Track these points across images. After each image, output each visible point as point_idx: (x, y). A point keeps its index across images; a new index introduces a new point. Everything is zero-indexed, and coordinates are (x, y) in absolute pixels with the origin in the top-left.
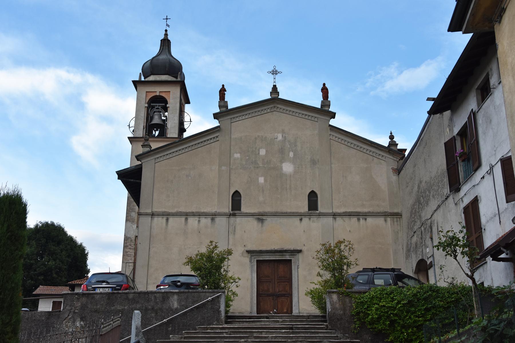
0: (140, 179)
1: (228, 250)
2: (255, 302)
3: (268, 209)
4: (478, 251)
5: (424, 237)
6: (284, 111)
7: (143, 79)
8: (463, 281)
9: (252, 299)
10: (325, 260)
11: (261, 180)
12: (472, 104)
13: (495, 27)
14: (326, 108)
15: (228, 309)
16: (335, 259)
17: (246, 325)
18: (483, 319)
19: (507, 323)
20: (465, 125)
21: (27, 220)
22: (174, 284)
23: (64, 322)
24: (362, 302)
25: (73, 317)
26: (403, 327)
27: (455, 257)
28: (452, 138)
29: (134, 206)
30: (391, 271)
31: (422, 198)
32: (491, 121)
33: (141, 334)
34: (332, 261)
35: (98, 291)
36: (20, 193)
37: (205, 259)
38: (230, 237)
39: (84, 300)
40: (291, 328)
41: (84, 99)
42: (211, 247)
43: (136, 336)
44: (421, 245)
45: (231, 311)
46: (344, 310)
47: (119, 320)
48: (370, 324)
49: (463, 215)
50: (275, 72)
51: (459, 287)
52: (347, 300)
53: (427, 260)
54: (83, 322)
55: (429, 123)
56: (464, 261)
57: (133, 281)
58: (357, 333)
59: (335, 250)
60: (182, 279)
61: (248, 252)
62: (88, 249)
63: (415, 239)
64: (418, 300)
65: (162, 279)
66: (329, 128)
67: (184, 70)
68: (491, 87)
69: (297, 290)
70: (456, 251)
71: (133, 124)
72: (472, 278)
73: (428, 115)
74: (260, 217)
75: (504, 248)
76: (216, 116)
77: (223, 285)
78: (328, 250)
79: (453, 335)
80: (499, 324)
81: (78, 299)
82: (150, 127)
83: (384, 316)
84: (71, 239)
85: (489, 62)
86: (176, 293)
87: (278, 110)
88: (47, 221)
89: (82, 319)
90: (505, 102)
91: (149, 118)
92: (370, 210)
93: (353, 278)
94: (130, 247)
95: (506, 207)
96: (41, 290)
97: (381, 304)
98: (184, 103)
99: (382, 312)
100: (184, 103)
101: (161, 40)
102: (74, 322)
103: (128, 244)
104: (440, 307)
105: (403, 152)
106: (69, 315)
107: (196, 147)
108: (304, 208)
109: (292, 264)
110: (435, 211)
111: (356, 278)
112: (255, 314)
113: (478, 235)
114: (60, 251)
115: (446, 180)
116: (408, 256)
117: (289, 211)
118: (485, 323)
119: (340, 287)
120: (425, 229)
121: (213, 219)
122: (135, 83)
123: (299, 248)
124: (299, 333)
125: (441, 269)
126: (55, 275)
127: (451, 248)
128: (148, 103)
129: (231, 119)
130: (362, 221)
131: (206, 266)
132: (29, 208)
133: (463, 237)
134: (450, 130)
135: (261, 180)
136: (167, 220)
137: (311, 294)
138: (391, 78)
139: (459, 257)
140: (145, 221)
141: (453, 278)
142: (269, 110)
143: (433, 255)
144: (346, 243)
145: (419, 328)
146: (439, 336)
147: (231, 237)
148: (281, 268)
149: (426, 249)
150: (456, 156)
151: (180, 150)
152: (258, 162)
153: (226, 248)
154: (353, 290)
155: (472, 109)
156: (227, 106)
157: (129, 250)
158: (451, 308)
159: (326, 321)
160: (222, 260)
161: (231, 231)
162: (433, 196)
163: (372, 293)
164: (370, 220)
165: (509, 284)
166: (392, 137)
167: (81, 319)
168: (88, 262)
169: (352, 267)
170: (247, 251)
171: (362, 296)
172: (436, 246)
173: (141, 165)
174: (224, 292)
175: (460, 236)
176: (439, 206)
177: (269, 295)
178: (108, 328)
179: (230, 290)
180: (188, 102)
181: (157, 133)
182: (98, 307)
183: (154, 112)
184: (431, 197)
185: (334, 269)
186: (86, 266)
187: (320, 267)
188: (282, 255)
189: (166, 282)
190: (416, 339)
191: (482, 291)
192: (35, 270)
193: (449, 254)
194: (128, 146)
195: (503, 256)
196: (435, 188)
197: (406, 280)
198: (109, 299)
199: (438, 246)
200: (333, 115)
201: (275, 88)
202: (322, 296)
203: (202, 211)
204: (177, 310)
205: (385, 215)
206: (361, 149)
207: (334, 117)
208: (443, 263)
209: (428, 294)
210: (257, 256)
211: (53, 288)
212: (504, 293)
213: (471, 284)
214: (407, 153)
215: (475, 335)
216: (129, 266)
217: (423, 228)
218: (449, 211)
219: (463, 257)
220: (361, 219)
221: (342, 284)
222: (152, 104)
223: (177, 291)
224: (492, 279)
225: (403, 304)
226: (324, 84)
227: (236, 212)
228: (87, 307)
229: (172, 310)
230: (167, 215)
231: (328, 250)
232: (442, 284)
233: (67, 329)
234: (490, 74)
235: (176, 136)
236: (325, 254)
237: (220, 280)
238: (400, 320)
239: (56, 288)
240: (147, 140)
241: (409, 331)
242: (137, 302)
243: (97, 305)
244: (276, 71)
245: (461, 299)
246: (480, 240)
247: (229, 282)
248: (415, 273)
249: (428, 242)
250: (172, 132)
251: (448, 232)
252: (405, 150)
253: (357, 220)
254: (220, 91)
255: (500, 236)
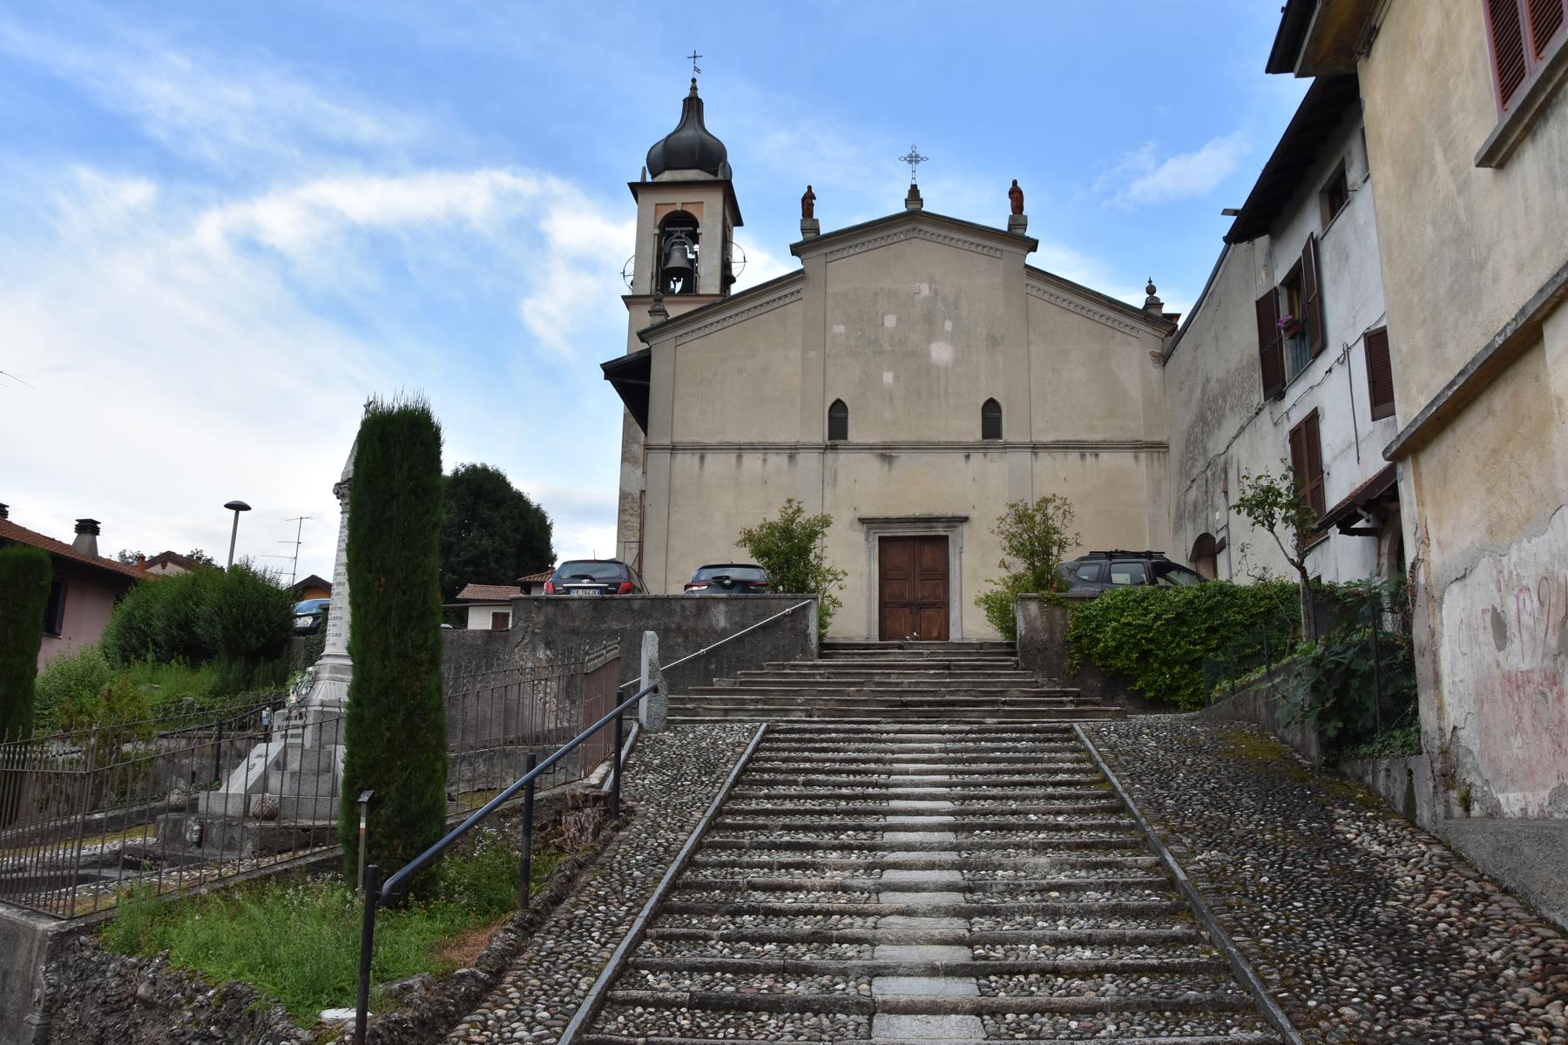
0: (648, 378)
1: (823, 517)
2: (877, 618)
3: (902, 436)
4: (1315, 515)
5: (1212, 489)
6: (934, 238)
7: (649, 179)
8: (1284, 574)
9: (869, 613)
10: (1015, 536)
11: (888, 378)
12: (1310, 222)
13: (1359, 64)
14: (1019, 231)
15: (822, 631)
16: (1036, 533)
17: (859, 661)
18: (1317, 643)
19: (1360, 649)
20: (1298, 265)
21: (442, 457)
22: (719, 582)
23: (516, 650)
24: (1086, 617)
25: (531, 641)
26: (1164, 663)
27: (1271, 527)
28: (1270, 292)
29: (636, 432)
30: (1145, 557)
31: (1209, 412)
32: (1347, 258)
33: (659, 673)
34: (1030, 537)
35: (574, 594)
36: (427, 406)
37: (777, 534)
38: (826, 491)
39: (550, 609)
40: (948, 667)
41: (545, 226)
42: (790, 511)
43: (650, 677)
44: (1207, 503)
45: (829, 635)
46: (1051, 631)
47: (617, 648)
48: (1101, 659)
49: (1288, 446)
50: (914, 159)
51: (1275, 586)
52: (1058, 613)
53: (1215, 536)
54: (551, 650)
55: (1225, 260)
56: (1287, 534)
57: (640, 576)
58: (1075, 676)
59: (1034, 516)
60: (735, 574)
61: (862, 521)
62: (552, 517)
63: (1193, 494)
64: (1196, 611)
65: (694, 573)
66: (1024, 271)
67: (730, 160)
68: (1350, 188)
69: (959, 594)
70: (1272, 516)
71: (631, 268)
72: (1300, 567)
73: (1224, 244)
74: (886, 452)
75: (1364, 509)
76: (796, 250)
77: (813, 584)
78: (1023, 517)
79: (1258, 676)
80: (1345, 651)
81: (539, 608)
82: (664, 275)
83: (1127, 642)
84: (519, 498)
85: (1345, 138)
86: (721, 599)
87: (922, 235)
88: (474, 462)
89: (548, 645)
90: (1377, 215)
91: (662, 256)
92: (1107, 436)
93: (1070, 571)
94: (631, 511)
95: (1371, 429)
96: (470, 591)
97: (1123, 620)
98: (730, 225)
99: (1125, 636)
100: (730, 225)
101: (684, 101)
102: (534, 650)
103: (627, 507)
104: (1237, 625)
105: (1174, 320)
106: (523, 638)
107: (757, 312)
108: (972, 430)
109: (950, 544)
110: (1235, 438)
111: (1076, 570)
112: (875, 640)
113: (1315, 484)
114: (499, 520)
115: (1258, 376)
116: (1178, 527)
117: (944, 439)
118: (1319, 650)
119: (1044, 588)
120: (1213, 474)
121: (791, 457)
122: (635, 188)
123: (963, 514)
124: (962, 675)
125: (1242, 551)
126: (493, 565)
127: (1263, 509)
128: (659, 227)
129: (826, 254)
130: (1089, 459)
131: (779, 547)
132: (444, 435)
133: (1288, 489)
134: (1267, 275)
135: (888, 378)
136: (702, 458)
137: (987, 603)
138: (1143, 174)
139: (1279, 526)
140: (659, 460)
141: (1264, 568)
142: (902, 237)
143: (1227, 526)
144: (1058, 502)
145: (1195, 664)
146: (1228, 677)
147: (828, 491)
148: (928, 555)
149: (1213, 514)
150: (1279, 328)
151: (724, 319)
152: (882, 341)
153: (818, 513)
154: (1071, 593)
155: (1312, 233)
156: (818, 230)
157: (629, 517)
158: (1258, 626)
159: (1014, 654)
160: (812, 535)
161: (829, 480)
162: (1232, 409)
163: (1108, 599)
164: (1105, 457)
165: (1368, 577)
166: (1151, 290)
167: (546, 645)
168: (553, 541)
169: (1068, 549)
170: (859, 519)
171: (1086, 605)
172: (1234, 507)
173: (649, 351)
174: (816, 599)
175: (1283, 486)
176: (1242, 429)
177: (903, 605)
178: (598, 662)
179: (827, 594)
180: (739, 223)
181: (679, 286)
182: (577, 624)
183: (673, 245)
184: (1227, 410)
185: (1033, 554)
186: (549, 548)
187: (1004, 549)
188: (931, 527)
189: (702, 578)
190: (1187, 685)
191: (1317, 592)
192: (458, 556)
193: (1259, 522)
194: (624, 313)
195: (1360, 524)
196: (1236, 392)
197: (1173, 575)
198: (595, 609)
199: (1239, 506)
200: (1033, 245)
201: (914, 191)
202: (1007, 606)
203: (771, 440)
204: (725, 633)
205: (1137, 446)
206: (1090, 315)
207: (1034, 249)
208: (1247, 541)
209: (1215, 600)
210: (880, 528)
211: (491, 588)
212: (1358, 594)
213: (1296, 578)
214: (1180, 323)
215: (1299, 674)
216: (631, 548)
217: (1209, 473)
218: (1262, 439)
219: (1287, 527)
220: (1088, 455)
221: (1048, 582)
222: (667, 229)
223: (724, 595)
224: (1337, 570)
225: (1166, 620)
226: (1015, 183)
227: (837, 442)
228: (556, 624)
229: (715, 632)
230: (702, 449)
231: (1023, 517)
232: (1243, 580)
233: (521, 663)
234: (1347, 161)
235: (717, 291)
236: (1016, 523)
237: (807, 574)
238: (1159, 649)
239: (497, 588)
240: (659, 301)
241: (1176, 671)
242: (649, 617)
243: (574, 621)
244: (917, 156)
245: (1276, 608)
246: (1318, 493)
247: (825, 580)
248: (1191, 560)
249: (1220, 500)
250: (709, 283)
251: (1260, 477)
252: (1178, 316)
253: (1079, 457)
254: (804, 199)
255: (1357, 486)
